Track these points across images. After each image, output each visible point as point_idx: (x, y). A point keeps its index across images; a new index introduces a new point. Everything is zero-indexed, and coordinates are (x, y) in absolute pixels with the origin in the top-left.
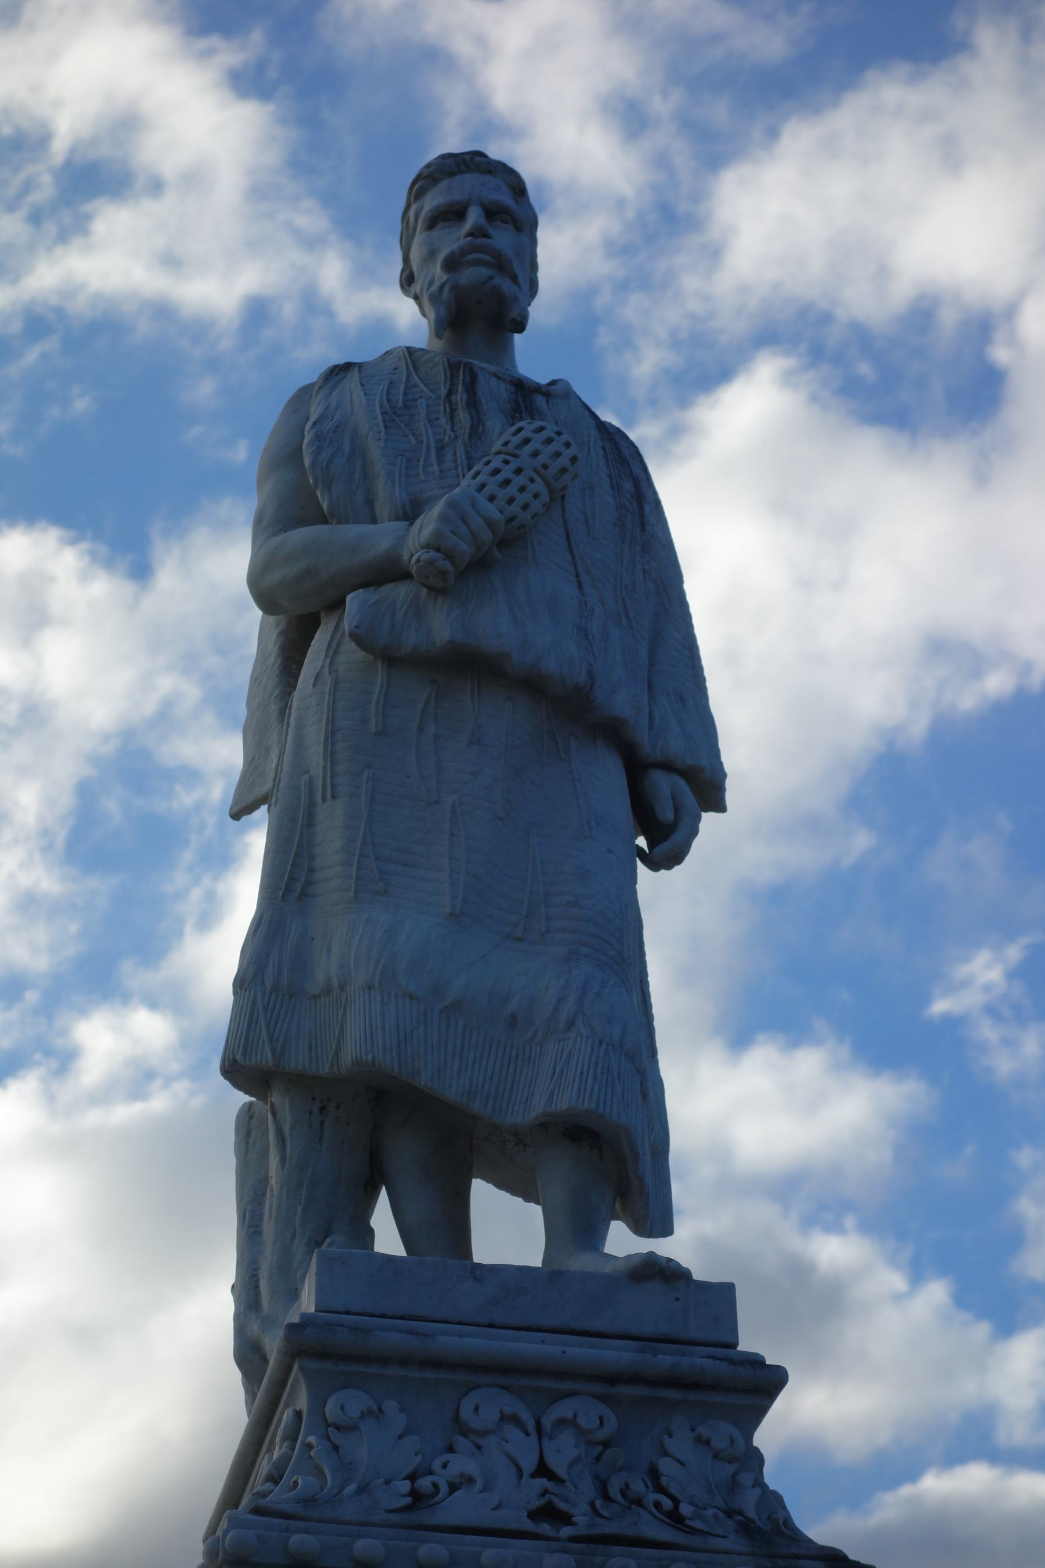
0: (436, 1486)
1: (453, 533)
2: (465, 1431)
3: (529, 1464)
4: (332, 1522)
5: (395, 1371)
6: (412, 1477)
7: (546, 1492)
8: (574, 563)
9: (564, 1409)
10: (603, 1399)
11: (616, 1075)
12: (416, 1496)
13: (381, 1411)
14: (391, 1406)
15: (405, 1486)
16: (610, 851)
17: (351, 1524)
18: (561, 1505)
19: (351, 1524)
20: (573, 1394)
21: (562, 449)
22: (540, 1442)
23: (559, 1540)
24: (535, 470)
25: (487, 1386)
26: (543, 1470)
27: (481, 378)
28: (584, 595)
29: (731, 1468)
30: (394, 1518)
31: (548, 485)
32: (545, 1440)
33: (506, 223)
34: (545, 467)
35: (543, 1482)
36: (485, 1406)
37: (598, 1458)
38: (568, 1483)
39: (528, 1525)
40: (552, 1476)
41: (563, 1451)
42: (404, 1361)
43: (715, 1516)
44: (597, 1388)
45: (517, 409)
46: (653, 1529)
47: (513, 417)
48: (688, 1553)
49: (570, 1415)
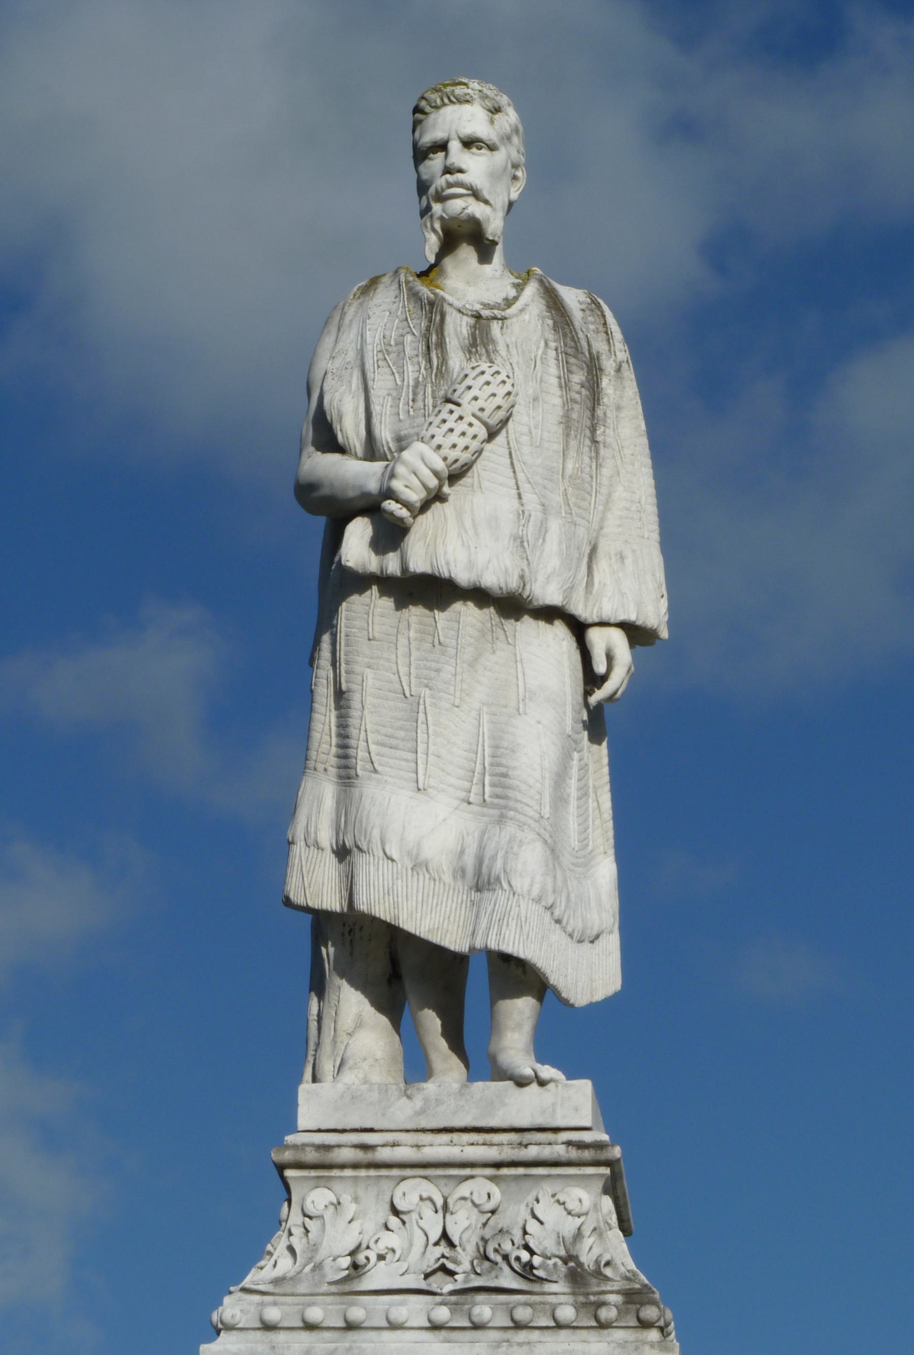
0: (367, 1258)
1: (407, 486)
2: (396, 1212)
3: (435, 1234)
4: (293, 1295)
5: (348, 1173)
6: (352, 1253)
7: (443, 1256)
8: (516, 478)
9: (465, 1189)
10: (492, 1179)
11: (523, 919)
12: (355, 1266)
13: (339, 1203)
14: (346, 1198)
15: (346, 1262)
16: (539, 722)
17: (304, 1295)
18: (450, 1266)
19: (304, 1295)
20: (472, 1177)
21: (506, 379)
22: (444, 1217)
23: (441, 1294)
24: (474, 415)
25: (414, 1177)
26: (445, 1236)
27: (448, 319)
28: (522, 505)
29: (578, 1221)
30: (334, 1289)
31: (485, 424)
32: (448, 1215)
33: (480, 149)
34: (482, 410)
35: (443, 1249)
36: (412, 1192)
37: (485, 1225)
38: (458, 1249)
39: (423, 1285)
40: (451, 1245)
41: (462, 1223)
42: (356, 1166)
43: (555, 1265)
44: (489, 1171)
45: (474, 344)
46: (508, 1280)
47: (470, 352)
48: (528, 1296)
49: (467, 1195)
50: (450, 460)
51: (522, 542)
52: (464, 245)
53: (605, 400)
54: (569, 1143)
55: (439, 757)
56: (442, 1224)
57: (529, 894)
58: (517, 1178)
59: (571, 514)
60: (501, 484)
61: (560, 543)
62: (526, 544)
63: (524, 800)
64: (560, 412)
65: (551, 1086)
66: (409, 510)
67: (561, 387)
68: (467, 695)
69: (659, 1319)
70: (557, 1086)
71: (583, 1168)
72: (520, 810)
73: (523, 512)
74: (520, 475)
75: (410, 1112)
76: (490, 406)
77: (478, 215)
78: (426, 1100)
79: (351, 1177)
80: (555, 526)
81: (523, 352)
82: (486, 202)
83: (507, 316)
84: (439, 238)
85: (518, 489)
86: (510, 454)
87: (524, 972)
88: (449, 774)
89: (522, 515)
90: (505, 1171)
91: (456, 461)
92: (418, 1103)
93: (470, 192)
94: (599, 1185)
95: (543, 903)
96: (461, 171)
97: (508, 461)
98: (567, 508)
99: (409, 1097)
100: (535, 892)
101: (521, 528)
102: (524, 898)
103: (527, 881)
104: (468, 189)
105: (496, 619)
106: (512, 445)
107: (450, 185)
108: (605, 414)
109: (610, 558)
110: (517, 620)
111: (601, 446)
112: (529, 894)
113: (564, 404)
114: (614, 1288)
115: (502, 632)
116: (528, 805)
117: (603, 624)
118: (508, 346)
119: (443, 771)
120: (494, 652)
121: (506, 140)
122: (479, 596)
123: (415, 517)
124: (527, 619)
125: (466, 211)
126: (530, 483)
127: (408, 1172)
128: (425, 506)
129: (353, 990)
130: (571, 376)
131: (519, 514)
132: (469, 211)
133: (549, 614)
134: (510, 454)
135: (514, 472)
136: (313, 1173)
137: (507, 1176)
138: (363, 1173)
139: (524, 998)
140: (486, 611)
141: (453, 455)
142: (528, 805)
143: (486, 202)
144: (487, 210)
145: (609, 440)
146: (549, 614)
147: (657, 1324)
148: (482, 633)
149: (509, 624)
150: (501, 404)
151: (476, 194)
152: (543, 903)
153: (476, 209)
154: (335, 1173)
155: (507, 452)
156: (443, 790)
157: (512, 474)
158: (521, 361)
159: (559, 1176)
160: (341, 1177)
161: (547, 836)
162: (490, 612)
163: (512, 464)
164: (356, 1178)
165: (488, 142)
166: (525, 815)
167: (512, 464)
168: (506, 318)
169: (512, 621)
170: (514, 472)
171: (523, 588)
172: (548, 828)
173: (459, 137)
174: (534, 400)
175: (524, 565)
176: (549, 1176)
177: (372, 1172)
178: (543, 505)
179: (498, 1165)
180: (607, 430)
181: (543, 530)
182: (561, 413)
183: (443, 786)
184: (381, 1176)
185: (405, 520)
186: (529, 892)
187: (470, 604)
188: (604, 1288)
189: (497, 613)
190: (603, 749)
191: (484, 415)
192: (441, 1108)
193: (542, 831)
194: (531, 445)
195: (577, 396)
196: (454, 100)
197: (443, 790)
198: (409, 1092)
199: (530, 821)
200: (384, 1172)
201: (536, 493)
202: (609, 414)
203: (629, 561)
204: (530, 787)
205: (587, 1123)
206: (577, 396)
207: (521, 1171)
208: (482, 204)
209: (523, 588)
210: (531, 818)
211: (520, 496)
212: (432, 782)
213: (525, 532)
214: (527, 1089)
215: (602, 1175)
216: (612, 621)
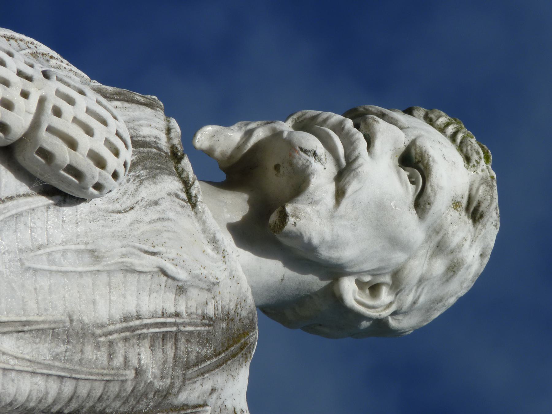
31: (36, 124)
33: (412, 183)
34: (57, 112)
52: (246, 196)
64: (88, 317)
67: (126, 319)
77: (314, 181)
81: (158, 233)
82: (340, 194)
83: (200, 207)
84: (239, 148)
93: (343, 162)
96: (370, 140)
104: (347, 157)
107: (339, 128)
113: (102, 326)
118: (156, 203)
121: (436, 239)
130: (146, 343)
132: (315, 166)
143: (340, 194)
144: (329, 198)
151: (344, 173)
153: (322, 175)
158: (144, 228)
165: (429, 189)
168: (194, 206)
173: (413, 142)
174: (92, 252)
182: (86, 320)
191: (49, 119)
194: (21, 251)
195: (119, 361)
196: (459, 140)
206: (119, 361)
208: (331, 188)
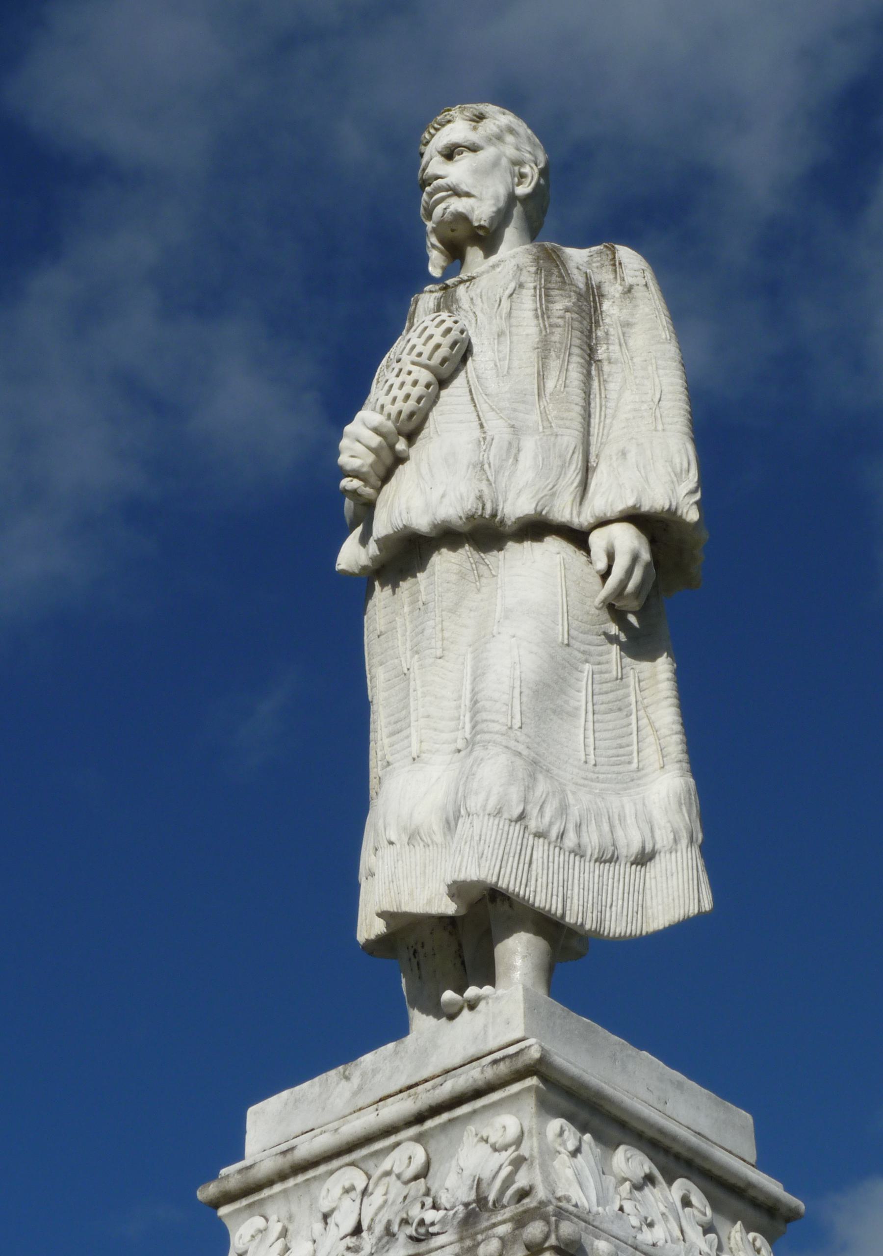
1: (352, 456)
5: (277, 1188)
16: (514, 637)
20: (398, 1144)
25: (341, 1167)
31: (426, 367)
34: (420, 355)
50: (393, 416)
51: (482, 468)
53: (607, 320)
54: (495, 1062)
55: (428, 717)
56: (357, 1211)
57: (484, 810)
58: (443, 1127)
59: (551, 427)
60: (461, 422)
61: (536, 457)
62: (486, 467)
63: (489, 718)
65: (482, 1006)
66: (361, 479)
67: (537, 317)
68: (452, 643)
69: (547, 1237)
70: (487, 1003)
71: (507, 1088)
72: (486, 729)
73: (484, 438)
74: (483, 407)
75: (348, 1094)
76: (427, 350)
77: (461, 209)
78: (363, 1075)
79: (280, 1192)
80: (529, 445)
81: (488, 298)
82: (468, 195)
83: (474, 275)
84: (441, 252)
85: (480, 419)
86: (470, 391)
87: (511, 906)
88: (442, 731)
89: (484, 440)
90: (430, 1124)
91: (400, 413)
92: (356, 1080)
93: (450, 193)
94: (530, 1104)
95: (506, 815)
97: (469, 398)
98: (546, 424)
99: (347, 1078)
100: (490, 807)
101: (482, 453)
102: (478, 815)
103: (482, 796)
104: (447, 191)
105: (476, 555)
106: (471, 382)
108: (607, 333)
109: (611, 459)
110: (501, 549)
111: (605, 363)
112: (484, 810)
114: (505, 1217)
115: (486, 567)
116: (494, 721)
117: (603, 523)
119: (435, 730)
120: (479, 590)
122: (448, 536)
123: (379, 490)
124: (511, 546)
125: (448, 210)
126: (493, 410)
127: (335, 1163)
128: (386, 478)
129: (424, 1016)
130: (550, 305)
131: (480, 441)
132: (452, 209)
133: (536, 528)
134: (470, 391)
135: (475, 406)
136: (244, 1202)
137: (431, 1129)
138: (291, 1182)
139: (515, 935)
140: (461, 551)
141: (393, 410)
142: (494, 721)
143: (468, 195)
145: (614, 356)
146: (536, 528)
147: (547, 1245)
148: (462, 576)
149: (493, 558)
150: (439, 342)
151: (456, 192)
152: (506, 815)
154: (266, 1193)
155: (467, 390)
156: (438, 751)
157: (473, 408)
159: (485, 1107)
160: (271, 1196)
161: (521, 748)
162: (466, 552)
163: (473, 399)
164: (285, 1191)
166: (491, 732)
167: (473, 399)
169: (495, 553)
170: (475, 406)
171: (483, 508)
172: (522, 738)
174: (499, 336)
175: (484, 486)
176: (474, 1112)
177: (300, 1178)
178: (513, 426)
179: (419, 1118)
180: (611, 347)
181: (513, 451)
182: (537, 340)
183: (437, 746)
184: (308, 1180)
185: (359, 491)
186: (484, 807)
187: (444, 551)
188: (494, 1221)
189: (475, 549)
190: (662, 668)
191: (424, 359)
192: (378, 1076)
193: (512, 744)
194: (498, 376)
195: (560, 322)
197: (438, 751)
198: (347, 1073)
199: (498, 738)
200: (311, 1174)
201: (501, 418)
202: (612, 331)
203: (632, 457)
204: (496, 701)
205: (519, 1034)
206: (560, 322)
207: (445, 1117)
208: (464, 199)
209: (483, 508)
210: (497, 733)
211: (482, 426)
212: (425, 746)
213: (486, 456)
214: (459, 1020)
215: (529, 1089)
216: (610, 515)
